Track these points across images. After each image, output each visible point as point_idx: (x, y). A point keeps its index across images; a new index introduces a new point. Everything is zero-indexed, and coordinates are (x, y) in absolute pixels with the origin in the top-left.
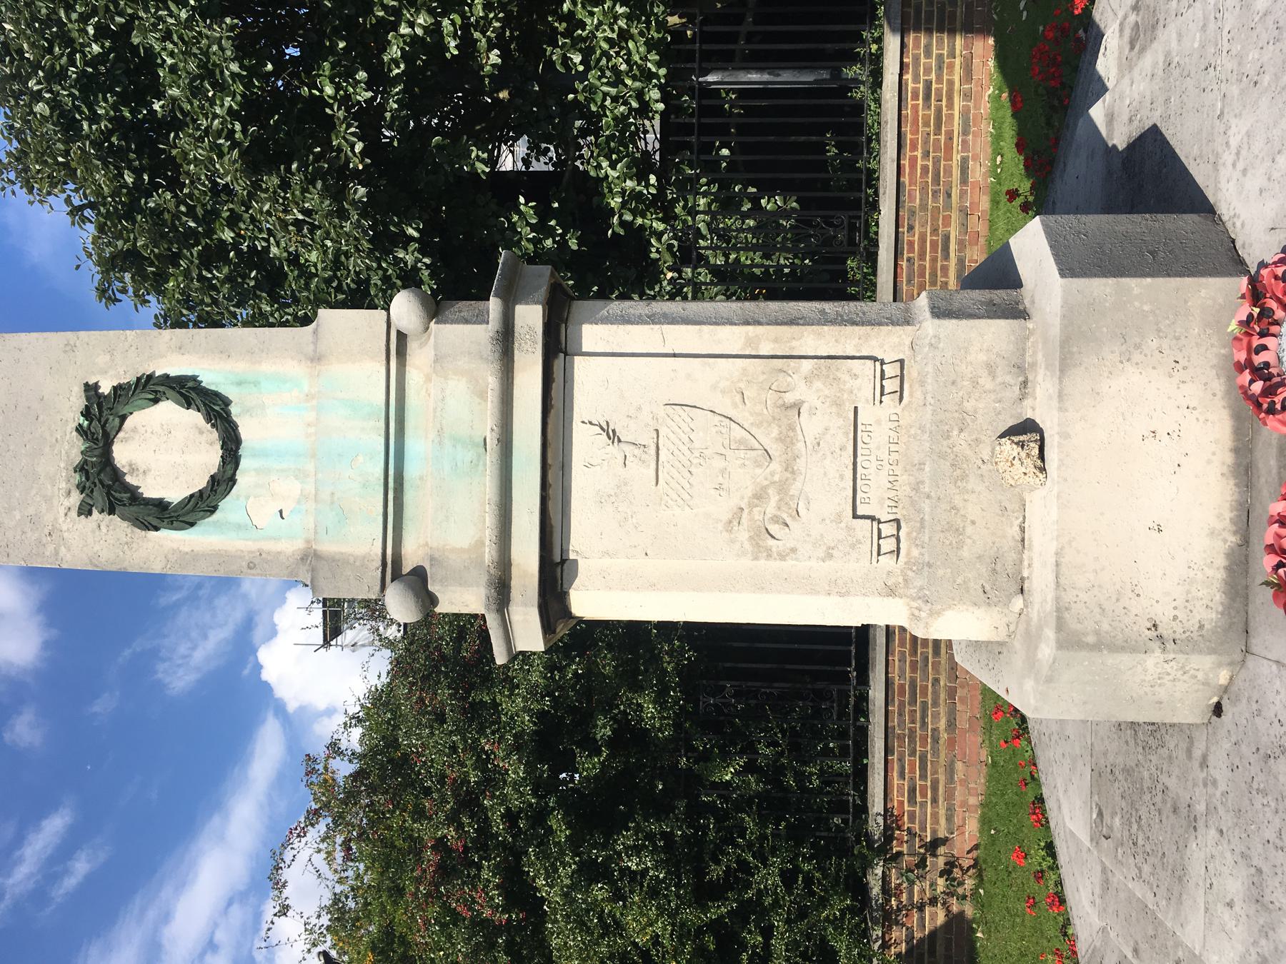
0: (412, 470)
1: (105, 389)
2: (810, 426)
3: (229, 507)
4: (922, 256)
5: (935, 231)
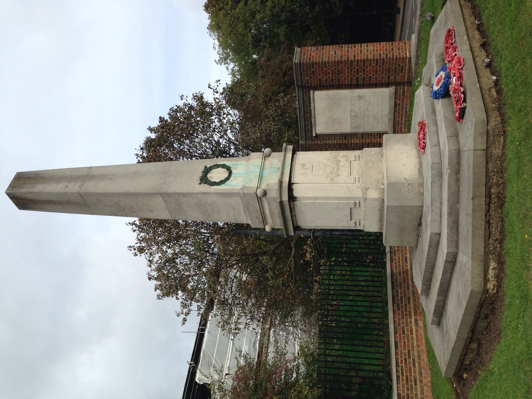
0: (264, 175)
1: (208, 166)
2: (342, 164)
3: (228, 182)
4: (399, 262)
5: (402, 256)
